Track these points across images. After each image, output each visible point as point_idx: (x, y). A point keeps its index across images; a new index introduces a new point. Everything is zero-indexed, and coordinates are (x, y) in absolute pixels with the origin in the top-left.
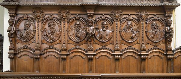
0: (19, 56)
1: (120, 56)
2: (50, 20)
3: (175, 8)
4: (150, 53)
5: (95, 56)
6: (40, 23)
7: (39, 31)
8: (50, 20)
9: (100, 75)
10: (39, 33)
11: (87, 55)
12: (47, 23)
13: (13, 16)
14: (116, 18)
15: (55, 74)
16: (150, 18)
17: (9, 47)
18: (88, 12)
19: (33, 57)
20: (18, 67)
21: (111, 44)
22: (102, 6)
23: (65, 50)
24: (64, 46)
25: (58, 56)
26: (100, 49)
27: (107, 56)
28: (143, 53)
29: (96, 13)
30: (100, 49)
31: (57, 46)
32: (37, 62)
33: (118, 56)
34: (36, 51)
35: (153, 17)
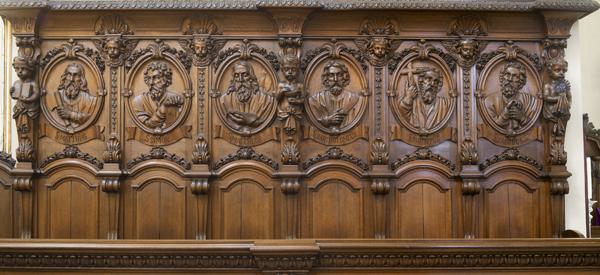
0: (49, 182)
1: (389, 181)
2: (68, 58)
3: (573, 21)
4: (492, 174)
5: (305, 182)
6: (474, 70)
7: (206, 96)
8: (68, 58)
9: (317, 248)
10: (205, 103)
11: (370, 179)
12: (142, 76)
13: (28, 45)
14: (377, 51)
15: (269, 244)
16: (406, 52)
17: (19, 150)
18: (281, 33)
19: (183, 186)
20: (310, 226)
21: (450, 140)
22: (60, 12)
23: (293, 163)
24: (113, 148)
25: (182, 184)
26: (143, 159)
27: (322, 183)
28: (471, 170)
29: (309, 35)
30: (143, 159)
31: (91, 147)
32: (474, 204)
33: (22, 181)
34: (375, 168)
35: (322, 50)
